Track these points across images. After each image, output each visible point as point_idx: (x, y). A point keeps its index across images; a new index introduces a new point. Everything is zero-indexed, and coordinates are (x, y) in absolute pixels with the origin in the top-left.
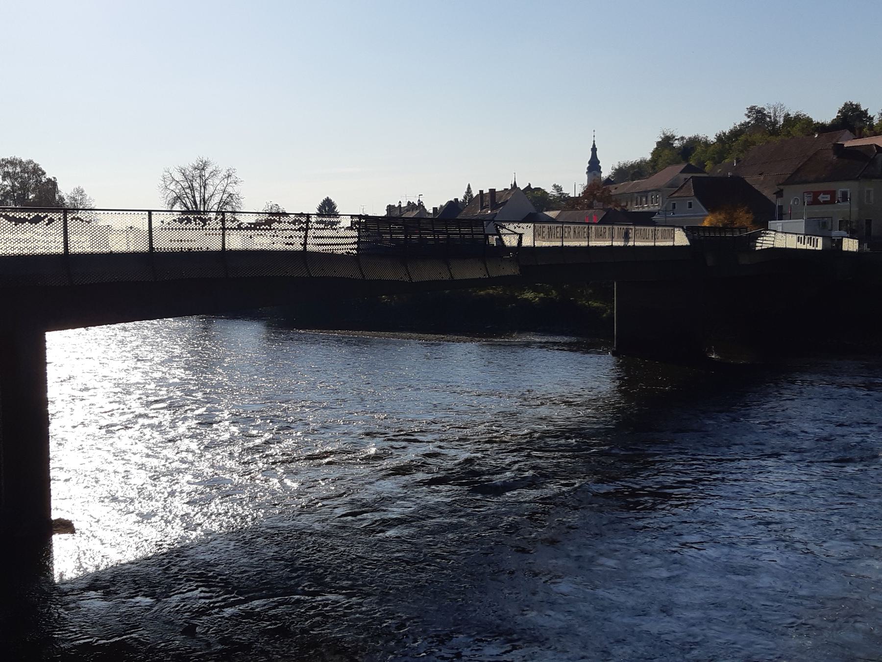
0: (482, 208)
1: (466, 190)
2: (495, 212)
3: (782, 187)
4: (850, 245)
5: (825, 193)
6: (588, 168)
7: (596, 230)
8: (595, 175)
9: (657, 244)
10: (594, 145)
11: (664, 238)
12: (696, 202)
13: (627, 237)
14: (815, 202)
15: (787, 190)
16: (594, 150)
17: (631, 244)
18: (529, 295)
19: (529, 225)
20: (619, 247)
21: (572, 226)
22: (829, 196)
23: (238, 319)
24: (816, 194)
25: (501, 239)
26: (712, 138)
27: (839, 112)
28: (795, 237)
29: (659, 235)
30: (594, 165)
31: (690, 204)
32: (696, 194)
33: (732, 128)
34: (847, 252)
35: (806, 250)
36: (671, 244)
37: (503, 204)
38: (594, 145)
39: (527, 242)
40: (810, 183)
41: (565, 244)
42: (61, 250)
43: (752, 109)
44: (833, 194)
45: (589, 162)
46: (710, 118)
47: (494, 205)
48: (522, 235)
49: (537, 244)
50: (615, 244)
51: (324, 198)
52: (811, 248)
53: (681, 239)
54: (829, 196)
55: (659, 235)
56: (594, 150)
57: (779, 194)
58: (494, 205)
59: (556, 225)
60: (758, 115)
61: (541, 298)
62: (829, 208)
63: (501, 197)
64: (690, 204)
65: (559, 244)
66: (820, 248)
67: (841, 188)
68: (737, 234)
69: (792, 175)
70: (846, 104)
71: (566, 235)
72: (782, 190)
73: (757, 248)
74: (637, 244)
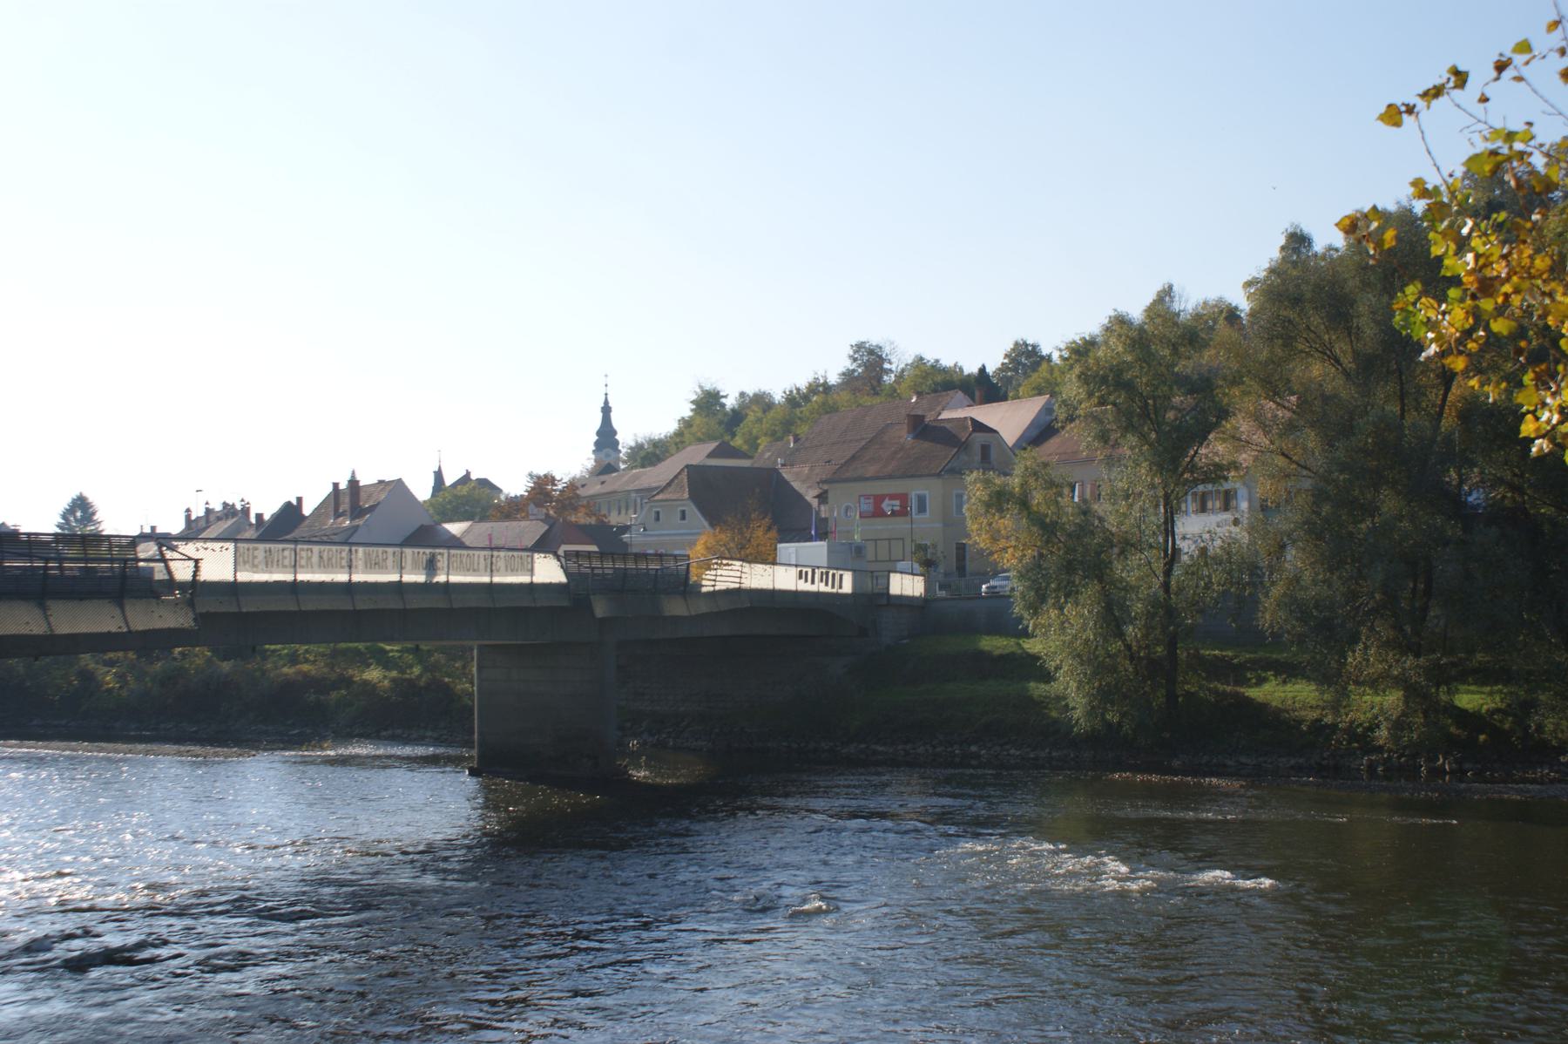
0: (337, 515)
1: (432, 483)
2: (357, 522)
3: (826, 487)
4: (906, 585)
5: (892, 497)
6: (596, 443)
7: (367, 555)
8: (608, 455)
9: (497, 580)
10: (606, 402)
11: (513, 570)
12: (692, 510)
13: (431, 566)
14: (878, 513)
15: (835, 492)
16: (606, 410)
17: (441, 578)
18: (373, 674)
19: (227, 545)
20: (415, 585)
21: (316, 548)
22: (897, 502)
23: (257, 749)
24: (879, 499)
25: (169, 572)
26: (778, 397)
27: (1006, 356)
28: (793, 572)
29: (501, 564)
30: (606, 436)
31: (683, 512)
32: (693, 497)
33: (811, 380)
34: (900, 597)
35: (818, 594)
36: (525, 579)
37: (372, 508)
38: (606, 402)
39: (209, 573)
40: (867, 479)
41: (300, 577)
42: (128, 608)
43: (859, 347)
44: (903, 498)
45: (598, 433)
46: (787, 357)
47: (357, 511)
48: (218, 564)
49: (244, 577)
50: (409, 578)
51: (74, 495)
52: (828, 589)
53: (548, 571)
54: (897, 502)
55: (501, 564)
56: (606, 410)
57: (822, 498)
58: (357, 511)
59: (281, 546)
60: (871, 360)
61: (393, 680)
62: (901, 525)
63: (370, 496)
64: (683, 512)
65: (289, 577)
66: (847, 588)
67: (915, 489)
68: (631, 565)
69: (842, 466)
70: (1016, 344)
71: (303, 562)
72: (826, 492)
73: (704, 590)
74: (454, 579)
